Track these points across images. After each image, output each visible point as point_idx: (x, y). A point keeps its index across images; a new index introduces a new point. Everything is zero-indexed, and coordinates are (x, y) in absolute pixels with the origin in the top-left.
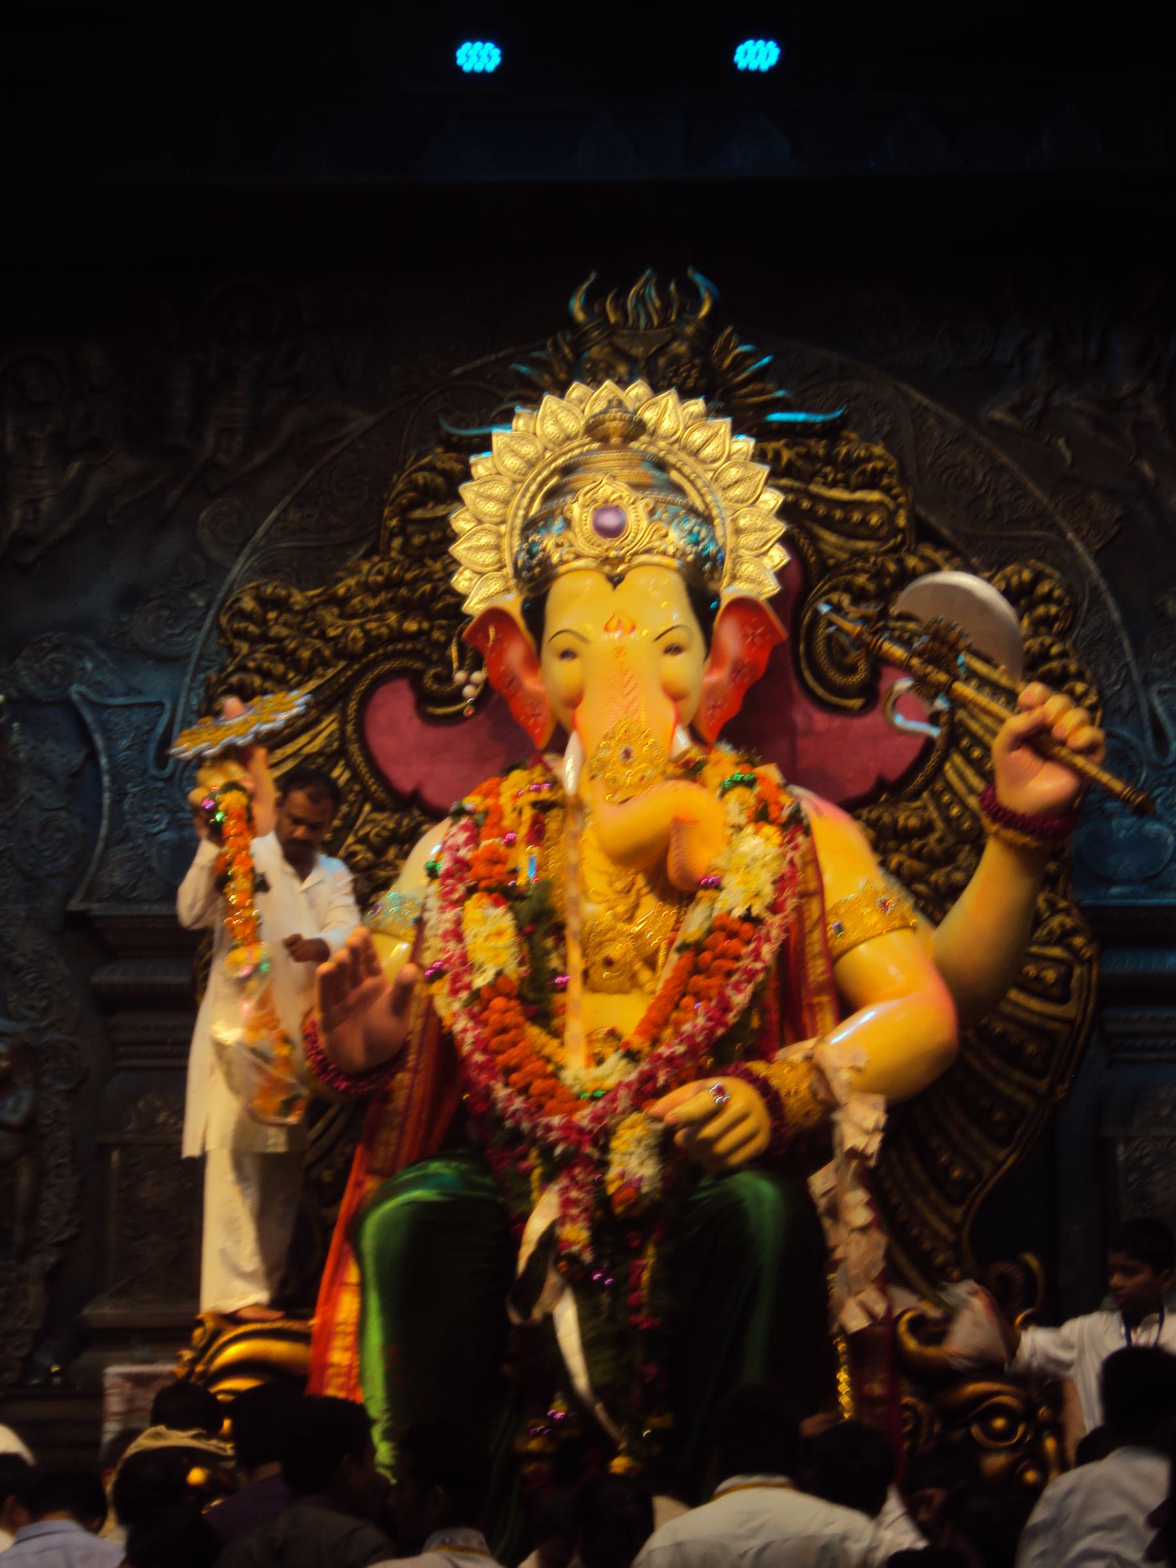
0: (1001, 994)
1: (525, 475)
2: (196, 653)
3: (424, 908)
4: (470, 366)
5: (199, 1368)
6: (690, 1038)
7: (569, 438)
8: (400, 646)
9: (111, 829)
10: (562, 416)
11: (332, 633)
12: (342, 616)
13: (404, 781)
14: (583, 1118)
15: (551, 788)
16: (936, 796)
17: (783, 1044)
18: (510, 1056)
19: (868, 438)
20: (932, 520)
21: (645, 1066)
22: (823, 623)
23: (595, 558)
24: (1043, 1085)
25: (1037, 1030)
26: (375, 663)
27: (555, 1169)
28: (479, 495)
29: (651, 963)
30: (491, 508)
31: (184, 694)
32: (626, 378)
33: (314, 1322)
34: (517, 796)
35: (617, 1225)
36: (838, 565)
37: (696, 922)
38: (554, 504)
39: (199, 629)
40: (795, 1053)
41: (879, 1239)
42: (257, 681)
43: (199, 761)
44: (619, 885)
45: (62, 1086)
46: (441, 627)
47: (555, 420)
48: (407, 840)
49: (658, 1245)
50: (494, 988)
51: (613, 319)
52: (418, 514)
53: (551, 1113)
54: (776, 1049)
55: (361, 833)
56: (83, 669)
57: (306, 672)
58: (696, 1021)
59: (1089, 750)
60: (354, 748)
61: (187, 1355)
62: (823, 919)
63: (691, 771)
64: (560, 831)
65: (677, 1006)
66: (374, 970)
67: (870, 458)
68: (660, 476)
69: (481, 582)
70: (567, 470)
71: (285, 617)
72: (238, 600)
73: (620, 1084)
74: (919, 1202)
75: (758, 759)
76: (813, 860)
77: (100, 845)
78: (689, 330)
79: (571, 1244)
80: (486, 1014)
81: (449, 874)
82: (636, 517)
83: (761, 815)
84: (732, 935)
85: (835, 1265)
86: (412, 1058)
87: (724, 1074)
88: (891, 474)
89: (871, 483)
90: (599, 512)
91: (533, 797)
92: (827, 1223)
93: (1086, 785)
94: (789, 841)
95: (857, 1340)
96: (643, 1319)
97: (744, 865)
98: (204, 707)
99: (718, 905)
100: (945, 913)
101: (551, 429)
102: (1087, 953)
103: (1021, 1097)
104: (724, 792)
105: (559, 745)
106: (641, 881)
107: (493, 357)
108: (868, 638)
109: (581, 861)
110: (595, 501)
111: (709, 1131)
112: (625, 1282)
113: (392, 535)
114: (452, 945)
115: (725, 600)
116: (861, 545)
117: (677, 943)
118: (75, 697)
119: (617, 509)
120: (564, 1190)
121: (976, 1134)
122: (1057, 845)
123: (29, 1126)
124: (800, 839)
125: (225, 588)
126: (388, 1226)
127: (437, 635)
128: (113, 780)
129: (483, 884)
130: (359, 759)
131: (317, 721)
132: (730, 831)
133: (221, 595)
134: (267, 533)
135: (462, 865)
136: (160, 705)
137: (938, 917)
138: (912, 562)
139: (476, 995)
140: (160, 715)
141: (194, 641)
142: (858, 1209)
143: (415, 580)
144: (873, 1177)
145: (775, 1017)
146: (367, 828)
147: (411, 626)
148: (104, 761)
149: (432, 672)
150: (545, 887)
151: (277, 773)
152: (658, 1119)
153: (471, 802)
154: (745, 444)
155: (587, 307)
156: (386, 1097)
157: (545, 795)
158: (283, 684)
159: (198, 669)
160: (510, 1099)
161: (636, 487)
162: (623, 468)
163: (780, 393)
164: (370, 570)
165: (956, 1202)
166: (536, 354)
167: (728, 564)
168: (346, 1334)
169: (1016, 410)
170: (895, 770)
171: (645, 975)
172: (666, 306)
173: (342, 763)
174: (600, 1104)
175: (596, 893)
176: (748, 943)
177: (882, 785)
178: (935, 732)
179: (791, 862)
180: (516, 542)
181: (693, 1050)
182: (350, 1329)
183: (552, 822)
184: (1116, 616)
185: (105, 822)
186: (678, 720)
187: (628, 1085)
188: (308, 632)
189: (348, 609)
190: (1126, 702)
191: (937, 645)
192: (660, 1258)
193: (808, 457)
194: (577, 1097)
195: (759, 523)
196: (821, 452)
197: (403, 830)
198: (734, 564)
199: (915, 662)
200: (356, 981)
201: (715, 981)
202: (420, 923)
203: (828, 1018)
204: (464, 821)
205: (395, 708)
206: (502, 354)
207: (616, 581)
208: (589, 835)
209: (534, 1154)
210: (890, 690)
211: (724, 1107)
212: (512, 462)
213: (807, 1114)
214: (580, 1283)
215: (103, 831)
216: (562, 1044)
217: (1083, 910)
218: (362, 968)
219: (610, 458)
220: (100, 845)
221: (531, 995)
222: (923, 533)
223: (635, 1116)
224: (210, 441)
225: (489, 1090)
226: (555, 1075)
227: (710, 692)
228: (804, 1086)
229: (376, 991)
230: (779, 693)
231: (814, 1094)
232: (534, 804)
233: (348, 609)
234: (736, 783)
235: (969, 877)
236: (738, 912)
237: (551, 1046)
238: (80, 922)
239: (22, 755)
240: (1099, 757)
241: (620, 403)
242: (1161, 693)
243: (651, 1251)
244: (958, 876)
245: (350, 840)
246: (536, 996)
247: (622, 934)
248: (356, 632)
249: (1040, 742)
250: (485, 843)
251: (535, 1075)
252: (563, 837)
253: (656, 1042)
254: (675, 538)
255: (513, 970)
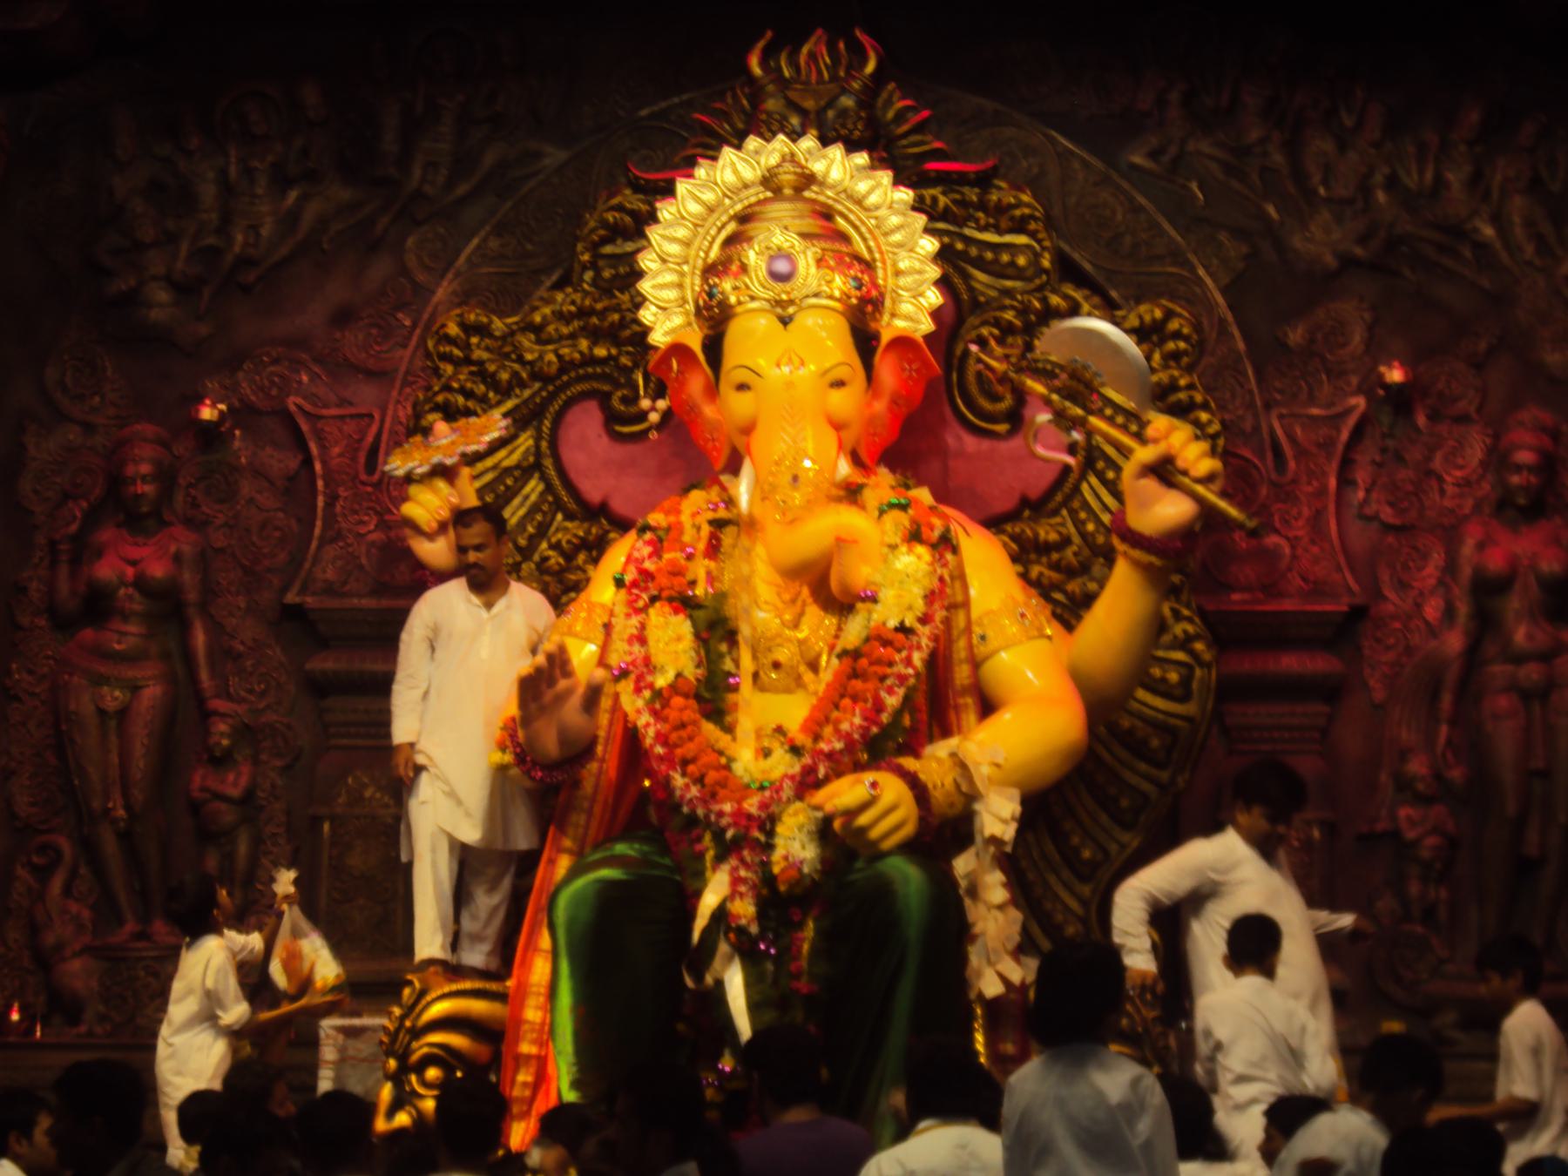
0: (1128, 694)
1: (704, 220)
2: (403, 369)
3: (612, 614)
4: (655, 108)
5: (408, 1024)
6: (847, 737)
7: (746, 186)
8: (590, 370)
9: (324, 529)
10: (741, 166)
11: (529, 357)
12: (539, 342)
13: (593, 491)
14: (752, 805)
15: (727, 508)
16: (1073, 513)
17: (931, 739)
18: (689, 749)
19: (1017, 187)
20: (1076, 256)
21: (807, 760)
22: (971, 362)
23: (768, 301)
24: (1164, 776)
25: (1160, 726)
26: (567, 385)
27: (726, 850)
28: (663, 237)
29: (814, 666)
30: (674, 249)
31: (391, 407)
32: (798, 128)
33: (509, 983)
34: (694, 515)
35: (780, 901)
36: (987, 303)
37: (855, 631)
38: (733, 251)
39: (405, 346)
40: (940, 750)
41: (1016, 915)
42: (461, 400)
43: (409, 479)
44: (787, 597)
45: (278, 763)
46: (628, 353)
47: (736, 168)
48: (596, 548)
49: (816, 920)
50: (674, 688)
51: (787, 74)
52: (608, 249)
53: (722, 801)
54: (922, 746)
55: (554, 540)
56: (300, 382)
57: (505, 392)
58: (852, 721)
59: (1208, 480)
60: (548, 463)
61: (397, 1011)
62: (968, 629)
63: (851, 493)
64: (734, 546)
65: (837, 707)
66: (567, 672)
67: (1019, 204)
68: (826, 225)
69: (665, 319)
70: (744, 218)
71: (488, 341)
72: (444, 326)
73: (785, 776)
74: (1052, 879)
75: (910, 482)
76: (961, 576)
77: (314, 544)
78: (856, 85)
79: (739, 917)
80: (666, 712)
81: (635, 584)
82: (806, 264)
83: (915, 536)
84: (886, 643)
85: (973, 939)
86: (599, 749)
87: (878, 768)
88: (1035, 219)
89: (1019, 227)
90: (772, 258)
91: (710, 515)
92: (968, 902)
93: (1207, 513)
94: (939, 559)
95: (994, 1007)
96: (803, 985)
97: (899, 579)
98: (411, 424)
99: (875, 616)
100: (1079, 618)
101: (729, 177)
102: (1207, 657)
103: (1146, 787)
104: (882, 513)
105: (734, 467)
106: (805, 592)
107: (676, 100)
108: (1012, 375)
109: (753, 571)
110: (768, 248)
111: (863, 820)
112: (787, 952)
113: (584, 268)
114: (637, 648)
115: (886, 337)
116: (1009, 284)
117: (838, 649)
118: (293, 408)
119: (789, 257)
120: (734, 870)
121: (1104, 818)
122: (1181, 561)
123: (248, 798)
124: (949, 556)
125: (430, 309)
126: (576, 901)
127: (624, 360)
128: (326, 485)
129: (665, 594)
130: (552, 473)
131: (514, 437)
132: (885, 550)
133: (426, 316)
134: (469, 260)
135: (647, 575)
136: (370, 416)
137: (1073, 622)
138: (1055, 300)
139: (658, 694)
140: (369, 426)
141: (402, 358)
142: (995, 888)
143: (606, 310)
144: (1011, 861)
145: (925, 717)
146: (560, 535)
147: (601, 352)
148: (318, 467)
149: (619, 394)
150: (721, 597)
151: (478, 484)
152: (818, 808)
153: (656, 518)
154: (905, 195)
155: (763, 63)
156: (577, 784)
157: (722, 513)
158: (486, 405)
159: (405, 383)
160: (687, 786)
161: (804, 236)
162: (794, 218)
163: (936, 145)
164: (564, 300)
165: (1083, 879)
166: (718, 105)
167: (888, 303)
168: (539, 994)
169: (1153, 155)
170: (1037, 487)
171: (808, 676)
172: (833, 68)
173: (537, 475)
174: (767, 793)
175: (766, 602)
176: (899, 651)
177: (1025, 502)
178: (1070, 460)
179: (941, 579)
180: (698, 281)
181: (850, 745)
182: (542, 990)
183: (728, 537)
184: (1241, 345)
185: (319, 523)
186: (840, 446)
187: (792, 778)
188: (507, 356)
189: (544, 336)
190: (1248, 425)
191: (1073, 383)
192: (818, 931)
193: (963, 203)
194: (747, 787)
195: (917, 265)
196: (975, 198)
197: (591, 538)
198: (894, 302)
199: (1055, 397)
200: (552, 682)
201: (870, 686)
202: (608, 627)
203: (970, 717)
204: (648, 536)
205: (585, 425)
206: (685, 97)
207: (785, 321)
208: (760, 550)
209: (707, 838)
210: (1033, 421)
211: (880, 800)
212: (694, 208)
213: (952, 805)
214: (747, 952)
215: (317, 531)
216: (734, 739)
217: (1202, 613)
218: (558, 672)
219: (781, 210)
220: (314, 544)
221: (707, 695)
222: (1068, 270)
223: (798, 805)
224: (417, 172)
225: (668, 779)
226: (727, 768)
227: (870, 421)
228: (949, 781)
229: (569, 692)
230: (931, 416)
231: (957, 786)
232: (711, 522)
233: (544, 336)
234: (892, 506)
235: (1102, 586)
236: (893, 623)
237: (723, 740)
238: (295, 614)
239: (243, 460)
240: (1216, 486)
241: (793, 155)
242: (1281, 417)
243: (811, 924)
244: (1092, 586)
245: (544, 545)
246: (712, 696)
247: (789, 640)
248: (551, 357)
249: (1164, 471)
250: (667, 556)
251: (709, 766)
252: (737, 552)
253: (817, 737)
254: (839, 283)
255: (691, 672)
